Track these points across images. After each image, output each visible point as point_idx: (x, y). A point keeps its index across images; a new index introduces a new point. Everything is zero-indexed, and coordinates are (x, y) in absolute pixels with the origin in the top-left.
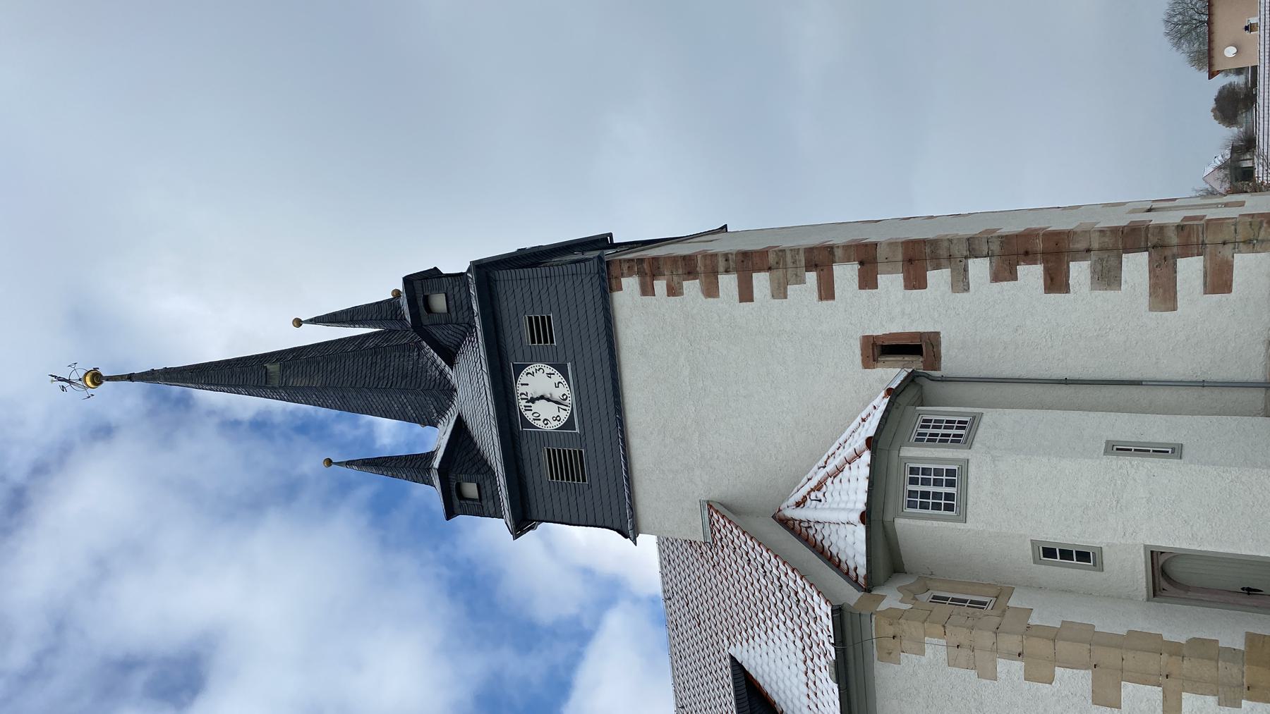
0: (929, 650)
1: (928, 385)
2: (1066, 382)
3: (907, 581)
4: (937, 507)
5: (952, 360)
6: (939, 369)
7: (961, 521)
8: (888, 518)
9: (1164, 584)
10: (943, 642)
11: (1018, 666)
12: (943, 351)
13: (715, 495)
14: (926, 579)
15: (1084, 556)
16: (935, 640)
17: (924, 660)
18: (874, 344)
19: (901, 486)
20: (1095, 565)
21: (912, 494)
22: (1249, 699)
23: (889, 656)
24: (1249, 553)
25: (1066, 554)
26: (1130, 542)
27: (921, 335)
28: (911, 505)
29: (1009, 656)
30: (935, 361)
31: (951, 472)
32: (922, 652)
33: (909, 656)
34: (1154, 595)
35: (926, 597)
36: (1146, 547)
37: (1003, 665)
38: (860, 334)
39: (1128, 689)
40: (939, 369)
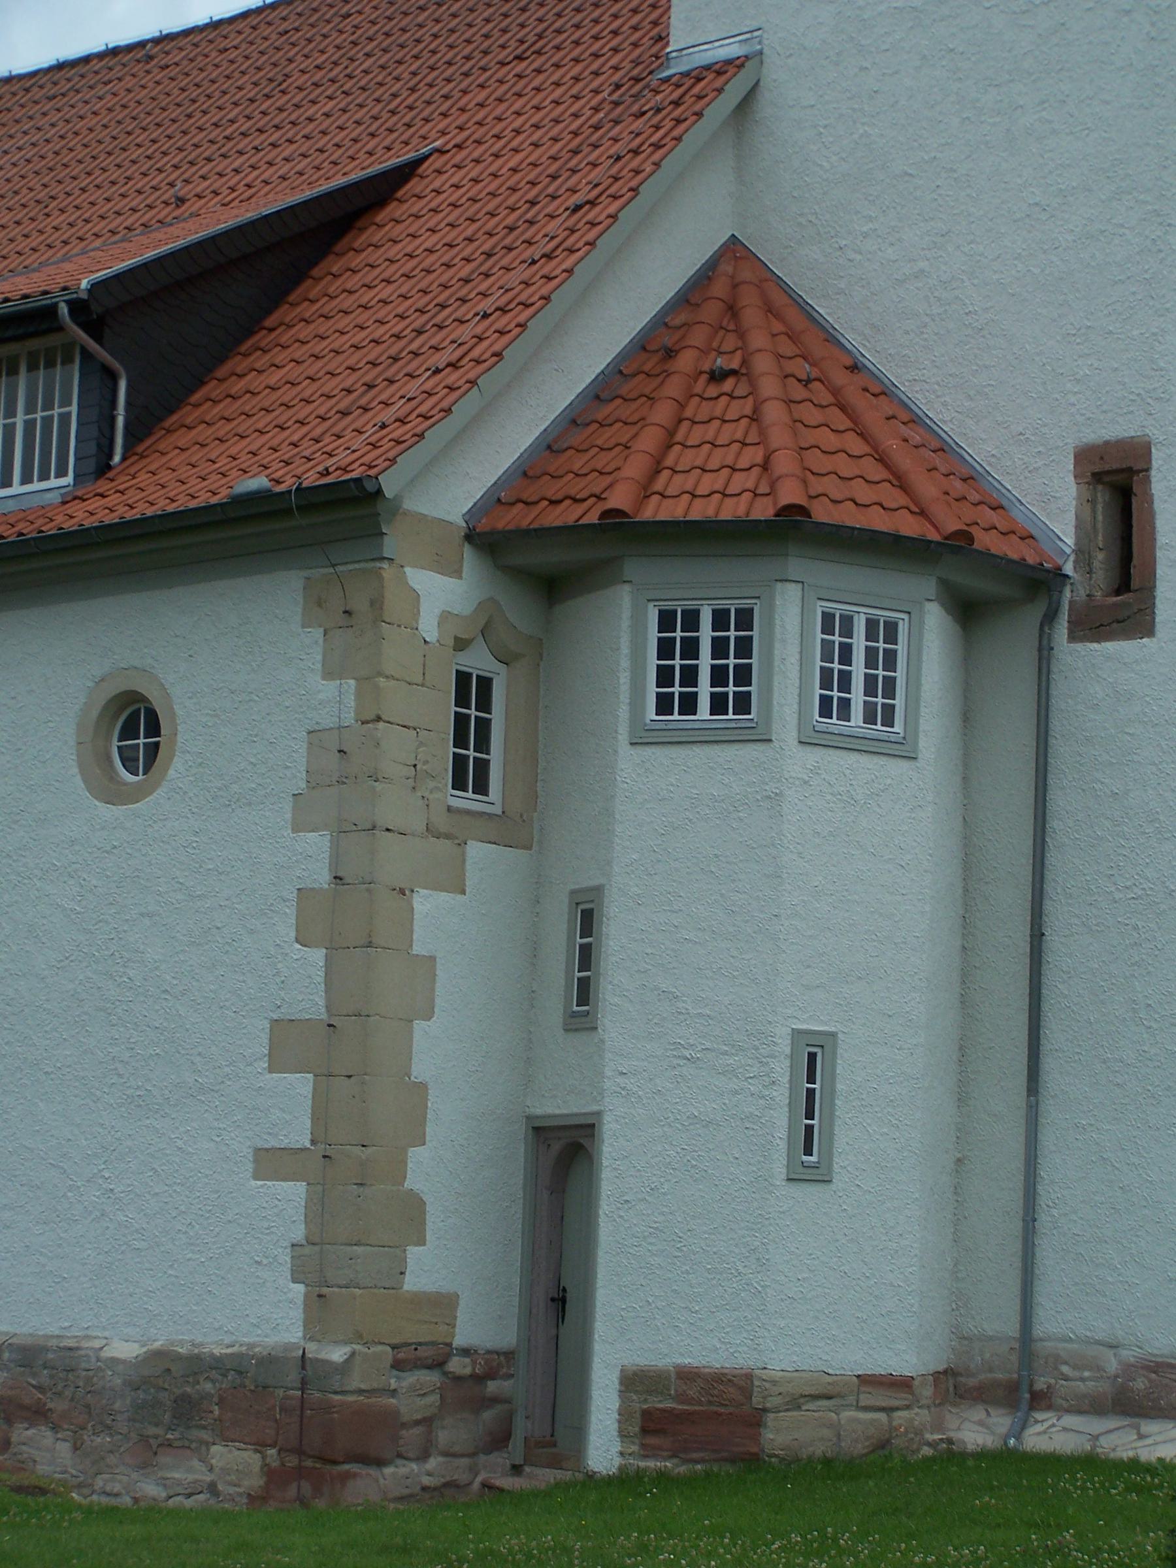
0: (329, 689)
1: (1036, 611)
2: (1037, 936)
3: (519, 613)
4: (744, 646)
5: (1095, 671)
6: (1072, 638)
7: (632, 733)
8: (633, 568)
9: (557, 1147)
10: (349, 718)
11: (322, 878)
12: (1110, 646)
13: (775, 73)
14: (535, 654)
15: (585, 992)
16: (350, 701)
17: (318, 678)
18: (1131, 472)
19: (706, 586)
20: (574, 1015)
21: (692, 620)
22: (306, 1295)
23: (316, 602)
24: (598, 1304)
25: (586, 957)
26: (608, 1084)
27: (1149, 589)
28: (666, 620)
29: (336, 858)
30: (1094, 625)
31: (743, 704)
32: (328, 675)
33: (320, 649)
34: (537, 1130)
35: (479, 661)
36: (598, 1114)
37: (317, 843)
38: (1155, 434)
39: (302, 1085)
40: (1072, 638)
